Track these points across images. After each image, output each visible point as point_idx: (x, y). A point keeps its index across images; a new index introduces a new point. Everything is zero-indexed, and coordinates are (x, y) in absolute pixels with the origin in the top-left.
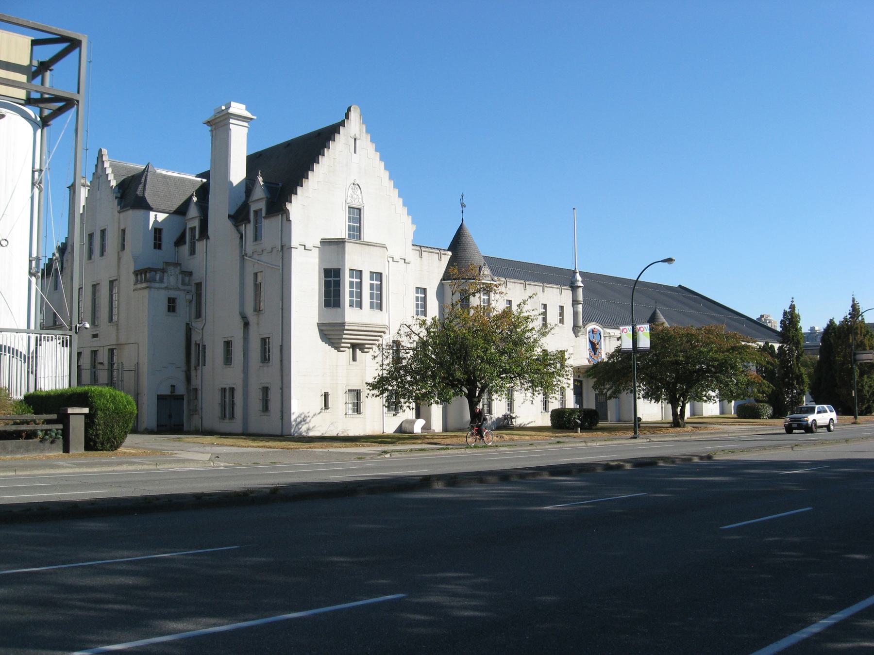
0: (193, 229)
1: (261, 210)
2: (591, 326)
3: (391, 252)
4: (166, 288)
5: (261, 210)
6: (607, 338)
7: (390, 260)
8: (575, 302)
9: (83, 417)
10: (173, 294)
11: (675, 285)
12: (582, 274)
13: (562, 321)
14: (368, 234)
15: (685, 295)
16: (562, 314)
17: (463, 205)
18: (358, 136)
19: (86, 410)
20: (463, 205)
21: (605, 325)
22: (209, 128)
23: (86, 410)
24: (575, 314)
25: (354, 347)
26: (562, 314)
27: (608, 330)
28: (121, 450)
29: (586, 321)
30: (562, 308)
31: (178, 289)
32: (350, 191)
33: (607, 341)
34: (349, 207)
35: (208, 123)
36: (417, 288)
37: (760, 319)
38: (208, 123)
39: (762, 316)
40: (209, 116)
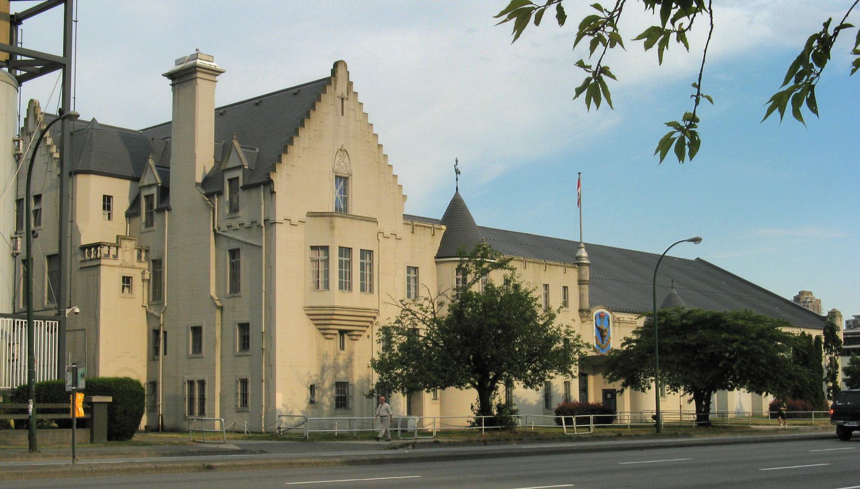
0: (149, 198)
1: (238, 178)
2: (596, 311)
3: (381, 226)
4: (121, 266)
5: (238, 178)
6: (617, 324)
7: (380, 236)
8: (581, 282)
9: (106, 406)
10: (128, 273)
11: (693, 258)
12: (589, 247)
13: (565, 304)
14: (355, 208)
15: (704, 270)
16: (565, 296)
17: (458, 172)
18: (345, 95)
19: (109, 399)
20: (458, 172)
21: (612, 310)
22: (170, 82)
23: (109, 399)
24: (581, 296)
25: (342, 333)
26: (565, 296)
27: (618, 315)
28: (136, 437)
29: (593, 304)
30: (565, 288)
31: (133, 267)
32: (338, 158)
33: (617, 328)
34: (336, 177)
35: (170, 76)
36: (409, 267)
37: (797, 298)
38: (170, 76)
39: (801, 293)
40: (172, 67)
